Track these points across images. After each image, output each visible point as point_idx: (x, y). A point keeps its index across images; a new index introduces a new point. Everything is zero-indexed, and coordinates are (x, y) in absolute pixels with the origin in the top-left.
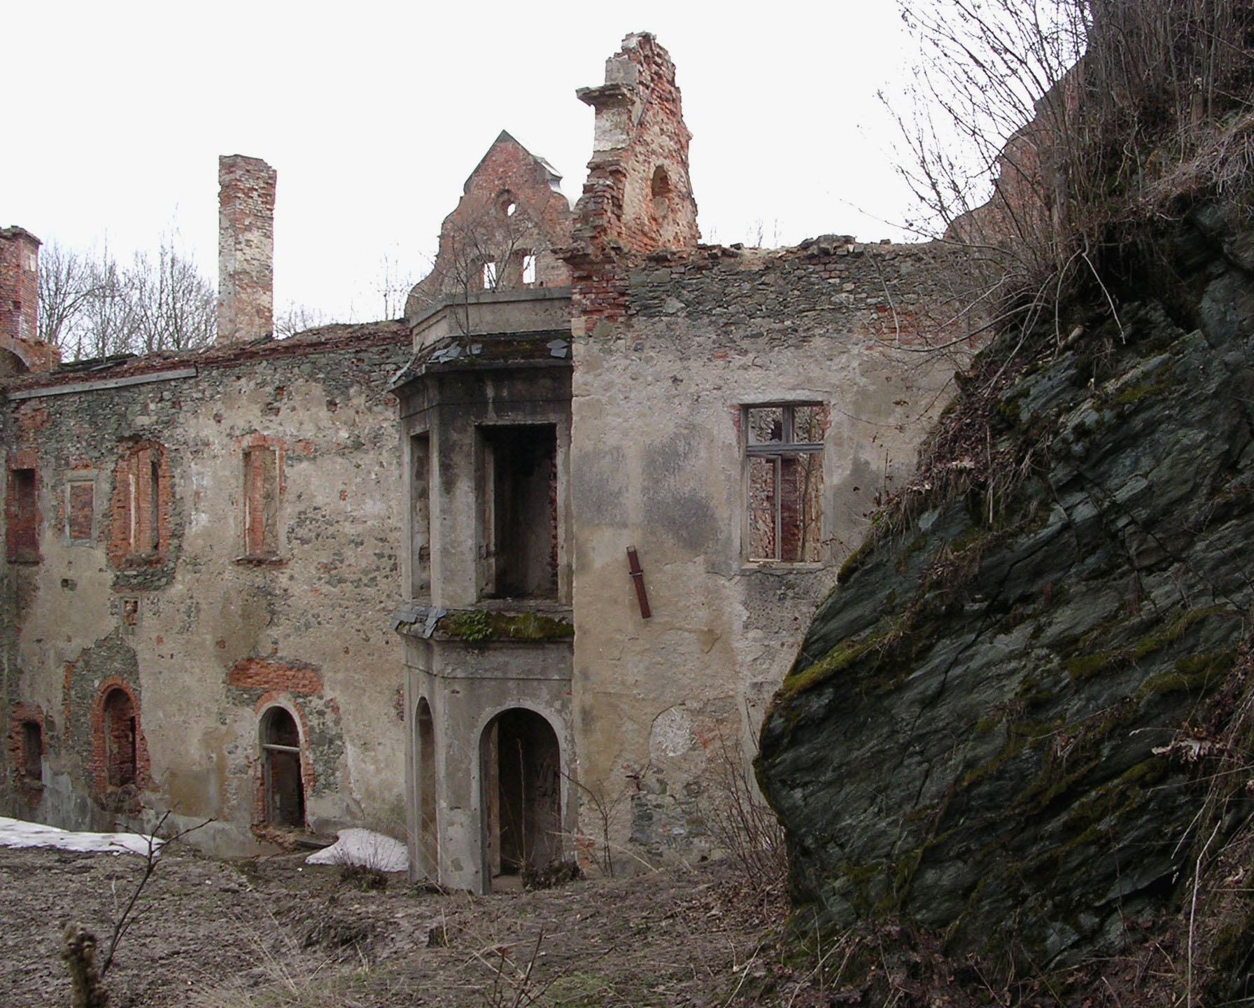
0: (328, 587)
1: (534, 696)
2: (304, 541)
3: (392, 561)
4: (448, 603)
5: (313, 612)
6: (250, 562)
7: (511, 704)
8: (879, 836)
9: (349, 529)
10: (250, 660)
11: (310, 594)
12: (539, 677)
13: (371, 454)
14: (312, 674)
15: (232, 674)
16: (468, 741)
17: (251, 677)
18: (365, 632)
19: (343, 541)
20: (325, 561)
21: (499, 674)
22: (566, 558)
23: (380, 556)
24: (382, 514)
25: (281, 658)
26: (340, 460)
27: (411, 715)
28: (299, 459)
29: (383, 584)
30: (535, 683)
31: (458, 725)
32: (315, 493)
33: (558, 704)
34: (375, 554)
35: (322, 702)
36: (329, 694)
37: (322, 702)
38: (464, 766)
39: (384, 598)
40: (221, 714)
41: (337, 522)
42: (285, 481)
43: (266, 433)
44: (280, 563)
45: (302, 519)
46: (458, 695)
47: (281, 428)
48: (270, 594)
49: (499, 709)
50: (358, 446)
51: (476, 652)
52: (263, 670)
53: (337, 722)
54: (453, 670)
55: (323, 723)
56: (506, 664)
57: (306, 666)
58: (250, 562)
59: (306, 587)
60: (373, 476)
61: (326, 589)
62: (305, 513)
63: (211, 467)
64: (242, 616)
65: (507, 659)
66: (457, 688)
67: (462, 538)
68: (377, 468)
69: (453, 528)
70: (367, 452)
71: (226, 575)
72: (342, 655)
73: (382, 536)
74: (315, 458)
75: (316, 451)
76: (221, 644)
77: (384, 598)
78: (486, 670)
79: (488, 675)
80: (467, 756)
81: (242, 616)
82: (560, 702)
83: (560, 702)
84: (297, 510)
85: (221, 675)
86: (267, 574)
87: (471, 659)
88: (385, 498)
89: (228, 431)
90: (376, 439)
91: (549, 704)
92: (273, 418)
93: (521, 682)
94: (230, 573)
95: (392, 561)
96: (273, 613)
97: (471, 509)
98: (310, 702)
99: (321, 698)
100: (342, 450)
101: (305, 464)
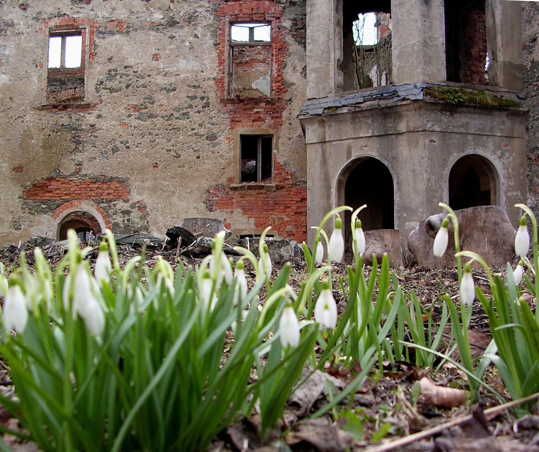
0: (137, 121)
1: (485, 146)
2: (112, 90)
3: (205, 101)
4: (427, 79)
5: (121, 139)
6: (55, 107)
7: (469, 151)
8: (354, 333)
9: (161, 80)
10: (50, 179)
11: (119, 127)
12: (488, 133)
13: (186, 29)
14: (118, 185)
15: (29, 191)
16: (442, 176)
17: (49, 192)
18: (175, 151)
19: (155, 89)
20: (135, 104)
21: (462, 130)
22: (502, 58)
23: (194, 98)
24: (196, 69)
25: (85, 175)
26: (154, 33)
27: (327, 179)
28: (112, 33)
29: (195, 117)
30: (485, 138)
31: (434, 165)
32: (126, 56)
33: (499, 153)
34: (188, 97)
35: (129, 204)
36: (135, 197)
37: (129, 204)
38: (438, 194)
39: (196, 126)
40: (15, 222)
41: (149, 76)
42: (95, 49)
43: (75, 16)
44: (88, 106)
45: (111, 75)
46: (434, 144)
47: (92, 13)
48: (75, 129)
49: (462, 155)
50: (172, 23)
51: (448, 113)
52: (64, 185)
53: (142, 218)
54: (433, 125)
55: (128, 220)
56: (468, 123)
57: (112, 179)
58: (55, 107)
59: (114, 122)
60: (187, 44)
61: (136, 122)
62: (115, 70)
63: (14, 41)
64: (44, 147)
65: (468, 120)
66: (434, 138)
67: (437, 36)
68: (191, 38)
69: (430, 28)
70: (182, 27)
71: (28, 118)
72: (151, 168)
73: (196, 84)
74: (128, 32)
75: (128, 27)
76: (18, 169)
77: (196, 126)
78: (454, 127)
79: (456, 130)
80: (440, 187)
81: (44, 147)
82: (500, 151)
83: (500, 151)
84: (107, 68)
85: (18, 191)
86: (73, 115)
87: (445, 118)
88: (198, 59)
89: (35, 15)
90: (191, 19)
91: (494, 152)
92: (85, 5)
93: (476, 137)
94: (31, 117)
95: (205, 101)
96: (78, 143)
97: (442, 17)
98: (115, 205)
99: (126, 201)
100: (156, 27)
101: (118, 37)
